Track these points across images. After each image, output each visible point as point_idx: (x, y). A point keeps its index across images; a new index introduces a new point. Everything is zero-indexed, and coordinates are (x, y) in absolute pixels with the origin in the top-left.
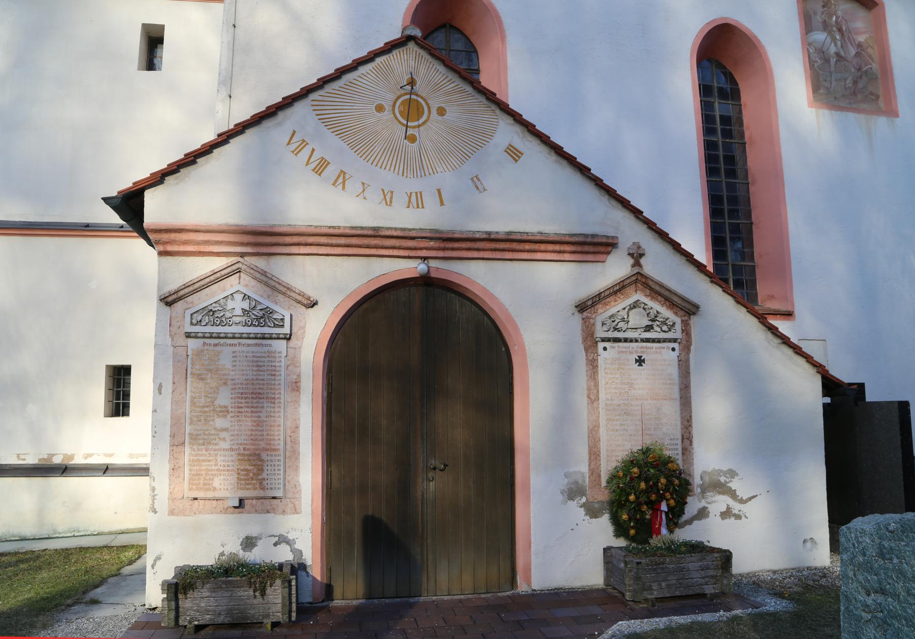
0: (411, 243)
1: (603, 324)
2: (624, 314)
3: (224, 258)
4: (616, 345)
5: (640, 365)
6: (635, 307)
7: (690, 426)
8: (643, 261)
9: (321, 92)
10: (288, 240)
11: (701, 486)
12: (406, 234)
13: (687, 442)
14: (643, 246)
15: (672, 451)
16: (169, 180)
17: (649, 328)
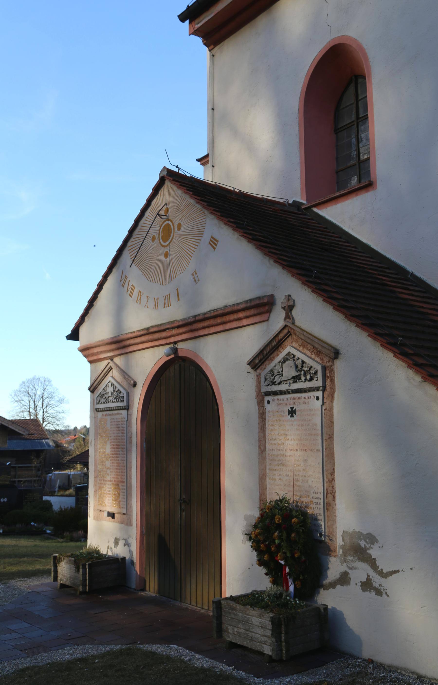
0: (164, 334)
1: (266, 379)
2: (278, 368)
3: (195, 328)
4: (276, 397)
5: (292, 416)
6: (287, 359)
7: (333, 480)
8: (294, 313)
9: (132, 240)
10: (132, 341)
11: (343, 547)
12: (162, 328)
13: (330, 497)
14: (294, 297)
15: (316, 509)
16: (86, 319)
17: (296, 379)
